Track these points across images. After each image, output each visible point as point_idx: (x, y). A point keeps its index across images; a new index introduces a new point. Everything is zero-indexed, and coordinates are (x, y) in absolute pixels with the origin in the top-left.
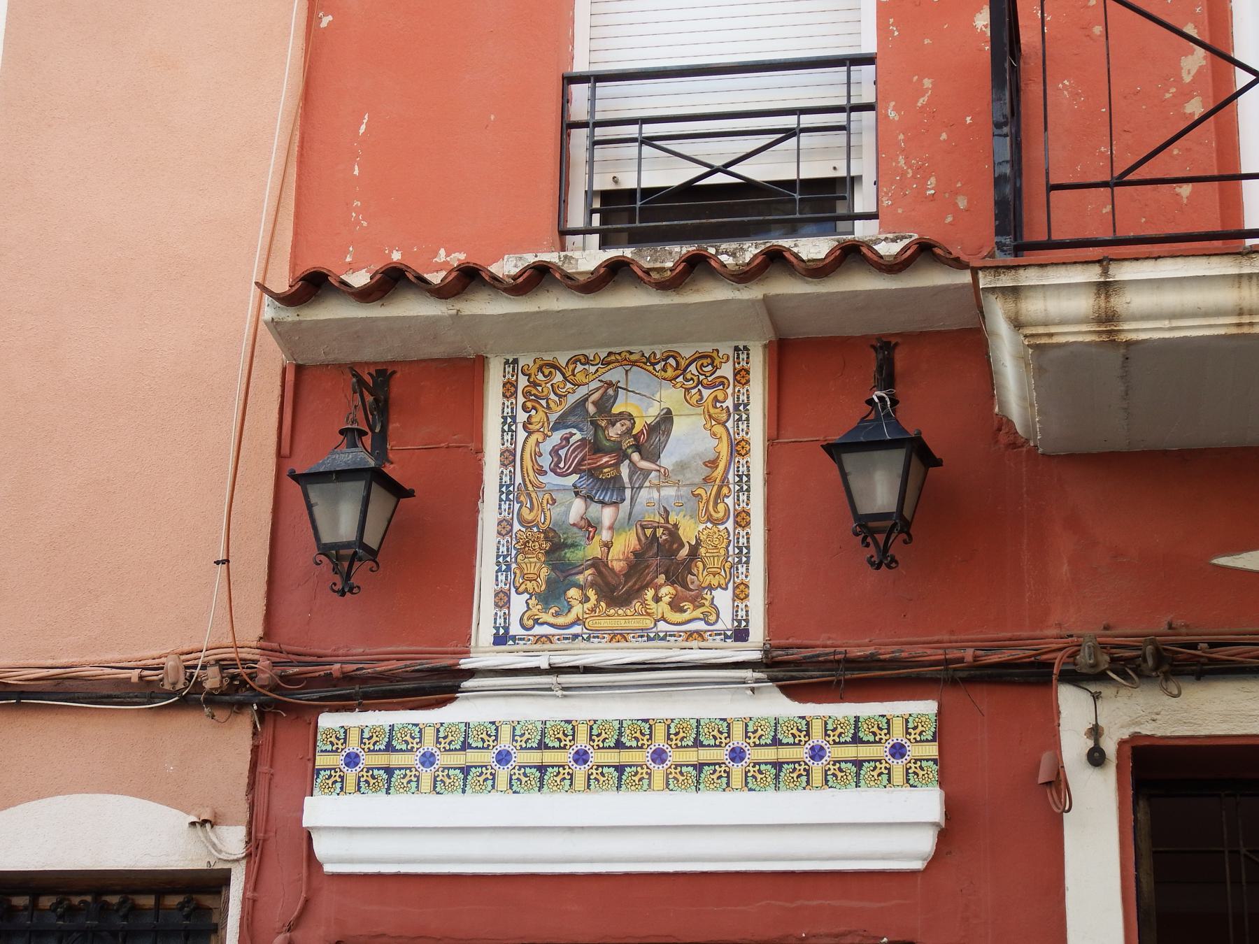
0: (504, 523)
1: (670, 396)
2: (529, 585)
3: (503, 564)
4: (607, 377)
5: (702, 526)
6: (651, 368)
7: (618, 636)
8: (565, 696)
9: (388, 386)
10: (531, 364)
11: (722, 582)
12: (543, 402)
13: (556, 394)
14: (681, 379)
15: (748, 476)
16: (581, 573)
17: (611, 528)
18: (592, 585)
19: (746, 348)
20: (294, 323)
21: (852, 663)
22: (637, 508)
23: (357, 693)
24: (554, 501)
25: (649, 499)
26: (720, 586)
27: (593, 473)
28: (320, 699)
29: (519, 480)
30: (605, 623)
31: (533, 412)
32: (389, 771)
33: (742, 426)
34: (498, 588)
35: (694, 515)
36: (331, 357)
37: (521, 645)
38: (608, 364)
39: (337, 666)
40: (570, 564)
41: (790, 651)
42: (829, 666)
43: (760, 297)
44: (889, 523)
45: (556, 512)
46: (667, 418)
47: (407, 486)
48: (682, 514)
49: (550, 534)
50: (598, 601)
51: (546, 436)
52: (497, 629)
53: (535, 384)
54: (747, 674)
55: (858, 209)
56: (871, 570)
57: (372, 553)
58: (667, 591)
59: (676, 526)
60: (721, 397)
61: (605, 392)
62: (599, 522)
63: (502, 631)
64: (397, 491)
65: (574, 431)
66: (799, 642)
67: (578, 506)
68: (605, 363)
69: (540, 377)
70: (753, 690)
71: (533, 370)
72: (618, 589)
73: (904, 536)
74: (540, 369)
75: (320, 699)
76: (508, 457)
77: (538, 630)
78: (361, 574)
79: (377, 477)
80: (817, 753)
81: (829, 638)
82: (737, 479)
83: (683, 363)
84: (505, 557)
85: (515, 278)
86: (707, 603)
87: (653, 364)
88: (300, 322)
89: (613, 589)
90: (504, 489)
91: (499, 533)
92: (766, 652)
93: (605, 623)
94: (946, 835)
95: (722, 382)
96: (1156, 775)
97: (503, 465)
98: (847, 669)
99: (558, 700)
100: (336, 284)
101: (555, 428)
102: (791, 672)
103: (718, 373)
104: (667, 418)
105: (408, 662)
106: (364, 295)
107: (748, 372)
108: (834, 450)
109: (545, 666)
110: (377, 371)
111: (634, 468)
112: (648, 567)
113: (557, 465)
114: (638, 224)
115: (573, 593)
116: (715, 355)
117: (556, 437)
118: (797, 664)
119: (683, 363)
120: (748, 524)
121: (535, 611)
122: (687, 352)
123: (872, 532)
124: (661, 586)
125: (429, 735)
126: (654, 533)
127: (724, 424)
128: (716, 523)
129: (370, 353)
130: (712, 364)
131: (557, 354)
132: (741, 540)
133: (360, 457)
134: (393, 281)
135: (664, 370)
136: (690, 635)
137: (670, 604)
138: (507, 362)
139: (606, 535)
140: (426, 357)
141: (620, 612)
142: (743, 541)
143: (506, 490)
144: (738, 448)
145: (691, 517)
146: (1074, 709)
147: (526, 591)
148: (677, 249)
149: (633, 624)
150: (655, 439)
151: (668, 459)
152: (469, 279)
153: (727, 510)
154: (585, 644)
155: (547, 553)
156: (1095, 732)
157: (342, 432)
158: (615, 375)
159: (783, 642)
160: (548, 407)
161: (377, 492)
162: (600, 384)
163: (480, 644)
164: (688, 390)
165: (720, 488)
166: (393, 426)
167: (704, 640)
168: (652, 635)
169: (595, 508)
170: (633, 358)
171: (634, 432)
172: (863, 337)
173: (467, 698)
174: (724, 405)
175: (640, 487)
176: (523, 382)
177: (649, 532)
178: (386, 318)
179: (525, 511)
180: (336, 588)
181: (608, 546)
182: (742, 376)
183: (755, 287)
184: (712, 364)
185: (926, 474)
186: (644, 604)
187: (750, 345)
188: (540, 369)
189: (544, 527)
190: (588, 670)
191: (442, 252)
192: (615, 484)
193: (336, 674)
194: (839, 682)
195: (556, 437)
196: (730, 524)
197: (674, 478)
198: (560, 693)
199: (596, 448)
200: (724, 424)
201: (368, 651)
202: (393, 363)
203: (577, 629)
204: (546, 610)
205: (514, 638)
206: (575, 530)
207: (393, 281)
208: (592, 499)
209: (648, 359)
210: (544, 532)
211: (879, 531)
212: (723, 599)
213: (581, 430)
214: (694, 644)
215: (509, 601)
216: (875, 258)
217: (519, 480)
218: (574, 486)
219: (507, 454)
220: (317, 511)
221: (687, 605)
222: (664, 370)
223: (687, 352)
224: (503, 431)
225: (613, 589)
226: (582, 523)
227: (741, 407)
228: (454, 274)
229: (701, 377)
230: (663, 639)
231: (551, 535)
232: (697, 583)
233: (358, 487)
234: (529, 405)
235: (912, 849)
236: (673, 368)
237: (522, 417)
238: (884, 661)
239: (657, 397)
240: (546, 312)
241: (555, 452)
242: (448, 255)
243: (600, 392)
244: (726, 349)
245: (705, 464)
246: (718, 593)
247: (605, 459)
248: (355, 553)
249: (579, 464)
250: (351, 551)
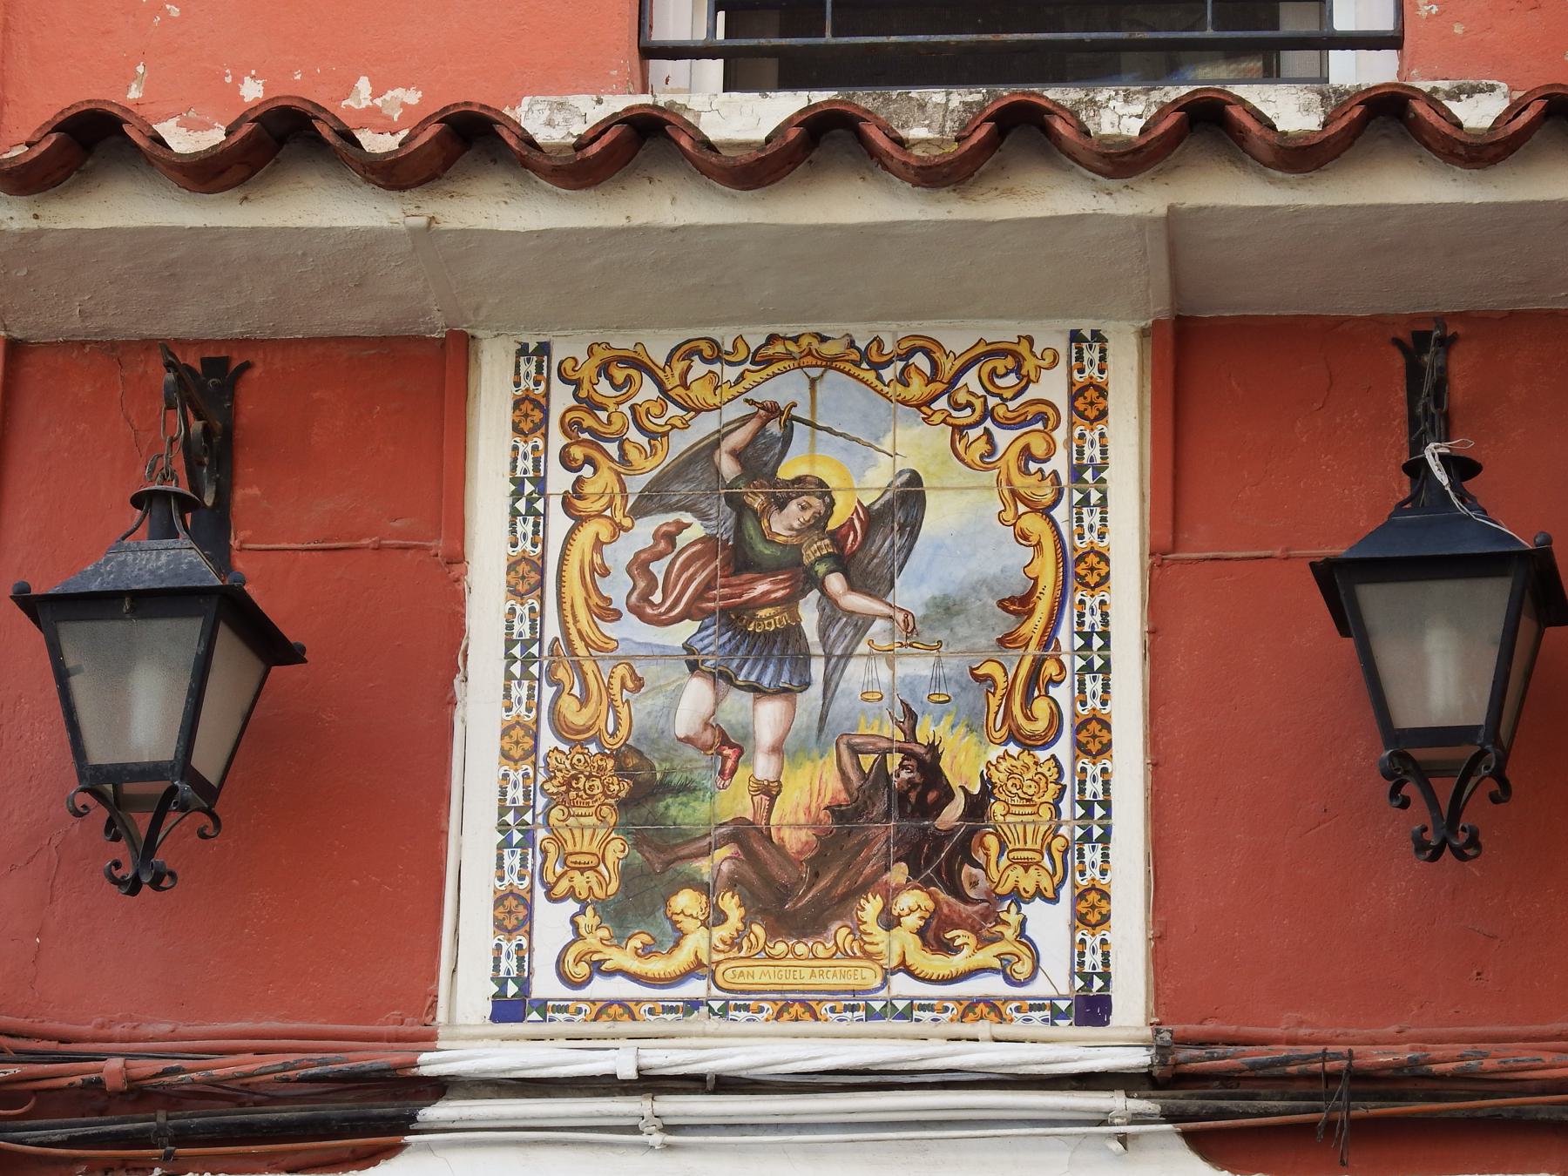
0: (518, 732)
1: (917, 445)
2: (580, 881)
3: (515, 832)
4: (765, 394)
5: (995, 752)
6: (870, 376)
7: (796, 1006)
8: (669, 1147)
9: (232, 398)
10: (582, 357)
11: (1046, 883)
12: (612, 449)
13: (642, 429)
14: (942, 403)
15: (1105, 636)
16: (707, 852)
17: (777, 749)
18: (734, 883)
19: (1097, 336)
20: (24, 236)
21: (1366, 1081)
22: (839, 705)
23: (160, 1130)
24: (639, 683)
25: (875, 683)
26: (1039, 893)
27: (734, 618)
28: (71, 1142)
29: (552, 630)
30: (761, 975)
31: (587, 471)
33: (1091, 518)
34: (503, 887)
35: (976, 724)
36: (94, 324)
37: (560, 1024)
38: (769, 361)
39: (115, 1064)
40: (681, 833)
41: (1220, 1050)
42: (1302, 1086)
43: (1160, 210)
44: (1467, 752)
45: (643, 708)
46: (910, 497)
47: (292, 635)
48: (947, 721)
49: (626, 760)
50: (746, 922)
51: (618, 529)
52: (502, 983)
53: (591, 405)
54: (1115, 1102)
55: (1343, 21)
56: (1419, 864)
57: (208, 792)
58: (913, 902)
59: (933, 748)
60: (1039, 448)
61: (763, 425)
62: (749, 735)
63: (512, 989)
64: (271, 646)
65: (687, 517)
66: (1231, 1029)
67: (696, 696)
68: (761, 360)
69: (604, 387)
70: (1123, 1139)
71: (587, 371)
72: (792, 895)
73: (1493, 786)
74: (604, 369)
75: (71, 1142)
76: (527, 576)
77: (601, 988)
78: (179, 840)
79: (233, 611)
81: (1300, 1024)
82: (1079, 642)
83: (948, 367)
84: (520, 811)
85: (581, 144)
86: (1009, 933)
87: (876, 367)
88: (39, 234)
89: (784, 893)
90: (516, 651)
91: (505, 755)
92: (1162, 1050)
93: (761, 975)
95: (1042, 415)
97: (514, 592)
98: (1354, 1096)
99: (650, 1158)
100: (143, 143)
101: (642, 508)
103: (1032, 393)
104: (910, 497)
105: (291, 1058)
106: (206, 175)
107: (1102, 392)
108: (1337, 581)
109: (627, 1072)
110: (204, 361)
111: (831, 610)
112: (867, 843)
113: (645, 597)
114: (829, 38)
115: (686, 901)
116: (1023, 349)
117: (644, 532)
118: (1227, 1080)
119: (948, 367)
120: (1106, 748)
121: (592, 941)
122: (957, 340)
123: (1423, 774)
124: (898, 890)
126: (882, 764)
127: (1046, 512)
128: (1028, 743)
129: (193, 318)
130: (1017, 370)
131: (644, 336)
132: (1089, 786)
133: (173, 560)
134: (285, 139)
135: (903, 380)
136: (969, 1008)
137: (921, 932)
138: (523, 351)
139: (764, 767)
140: (327, 331)
141: (801, 949)
142: (1093, 788)
143: (521, 652)
144: (1084, 569)
145: (971, 729)
147: (571, 893)
148: (937, 96)
149: (832, 979)
150: (884, 543)
151: (913, 591)
152: (469, 141)
153: (1056, 715)
154: (715, 1024)
155: (623, 805)
157: (138, 501)
158: (786, 389)
159: (1193, 1029)
160: (624, 458)
161: (228, 646)
162: (750, 409)
163: (460, 1018)
164: (959, 430)
165: (1038, 664)
166: (245, 494)
167: (1002, 1019)
168: (877, 1006)
169: (736, 704)
170: (828, 349)
171: (833, 524)
172: (1372, 318)
173: (428, 1147)
174: (1048, 468)
175: (847, 656)
176: (561, 398)
177: (867, 761)
178: (254, 231)
179: (569, 706)
180: (118, 874)
181: (770, 791)
182: (1089, 401)
183: (1148, 188)
184: (1017, 370)
185: (1539, 636)
186: (857, 931)
187: (1108, 328)
188: (604, 369)
189: (614, 744)
190: (726, 1084)
191: (364, 85)
192: (787, 644)
193: (114, 1082)
194: (1330, 1125)
195: (644, 532)
196: (1063, 749)
197: (927, 636)
198: (657, 1138)
199: (739, 558)
200: (1046, 512)
201: (183, 1029)
202: (244, 343)
203: (695, 988)
204: (619, 940)
205: (542, 1006)
206: (690, 751)
207: (285, 139)
208: (730, 680)
209: (864, 355)
210: (617, 756)
211: (1444, 770)
212: (1049, 924)
213: (703, 516)
214: (983, 1028)
215: (530, 917)
216: (1446, 128)
217: (552, 630)
218: (688, 647)
219: (523, 568)
220: (78, 684)
221: (961, 936)
222: (903, 380)
223: (957, 340)
224: (515, 513)
225: (784, 893)
226: (708, 736)
227: (1087, 474)
228: (433, 129)
229: (992, 402)
230: (905, 1015)
231: (632, 761)
232: (984, 884)
233: (185, 632)
234: (577, 452)
236: (925, 377)
237: (559, 480)
238: (1441, 1077)
239: (886, 444)
240: (644, 231)
241: (640, 566)
242: (375, 94)
243: (751, 426)
244: (1051, 336)
245: (1001, 604)
246: (1035, 911)
247: (761, 587)
248: (173, 790)
249: (700, 596)
250: (158, 788)
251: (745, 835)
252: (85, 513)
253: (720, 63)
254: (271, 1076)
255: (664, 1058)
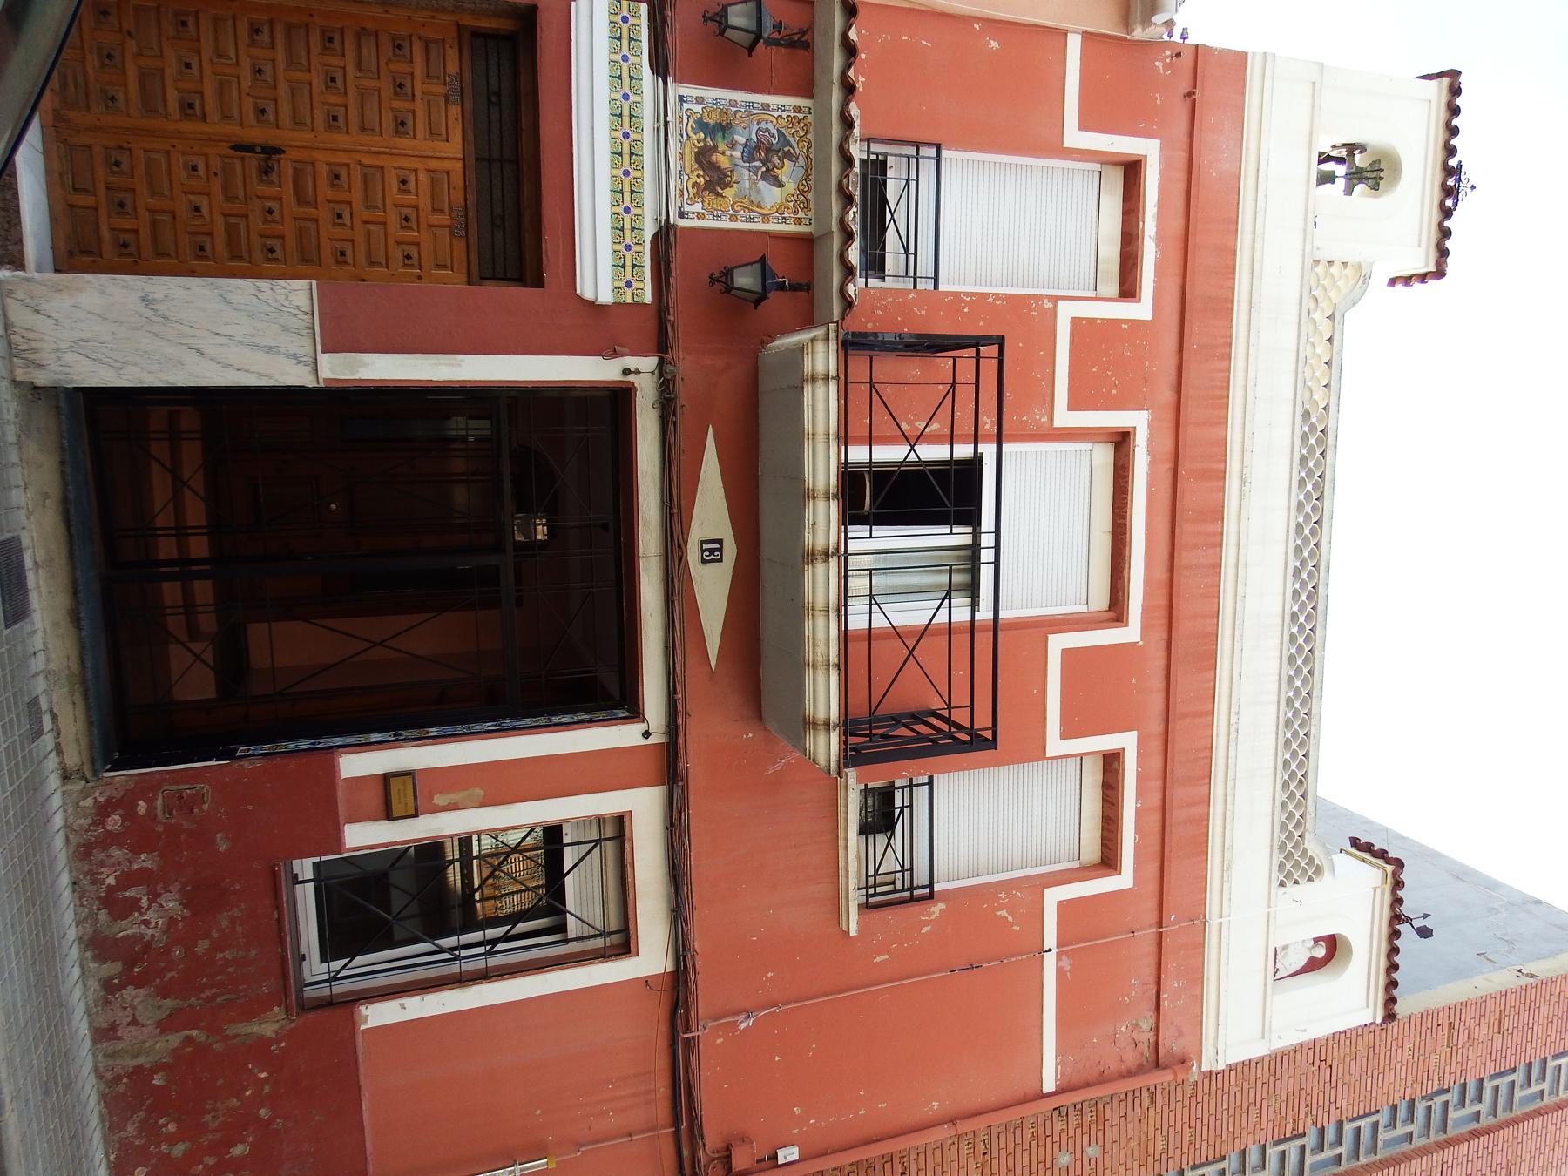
1: (790, 187)
3: (716, 101)
7: (682, 156)
25: (744, 174)
27: (757, 148)
32: (620, 39)
35: (736, 195)
41: (711, 514)
45: (740, 129)
46: (781, 185)
57: (722, 33)
67: (742, 140)
72: (704, 157)
78: (712, 26)
80: (628, 248)
94: (591, 304)
95: (796, 212)
96: (619, 398)
102: (665, 237)
104: (781, 185)
108: (763, 260)
111: (758, 168)
117: (774, 131)
122: (810, 196)
125: (636, 60)
133: (768, 31)
134: (850, 50)
143: (751, 104)
146: (648, 363)
151: (761, 184)
156: (638, 372)
158: (801, 161)
176: (801, 116)
182: (799, 221)
192: (751, 159)
195: (774, 131)
199: (769, 150)
212: (698, 207)
235: (585, 289)
251: (715, 147)
252: (778, 8)
253: (1057, 424)
254: (846, 1159)
255: (671, 126)
